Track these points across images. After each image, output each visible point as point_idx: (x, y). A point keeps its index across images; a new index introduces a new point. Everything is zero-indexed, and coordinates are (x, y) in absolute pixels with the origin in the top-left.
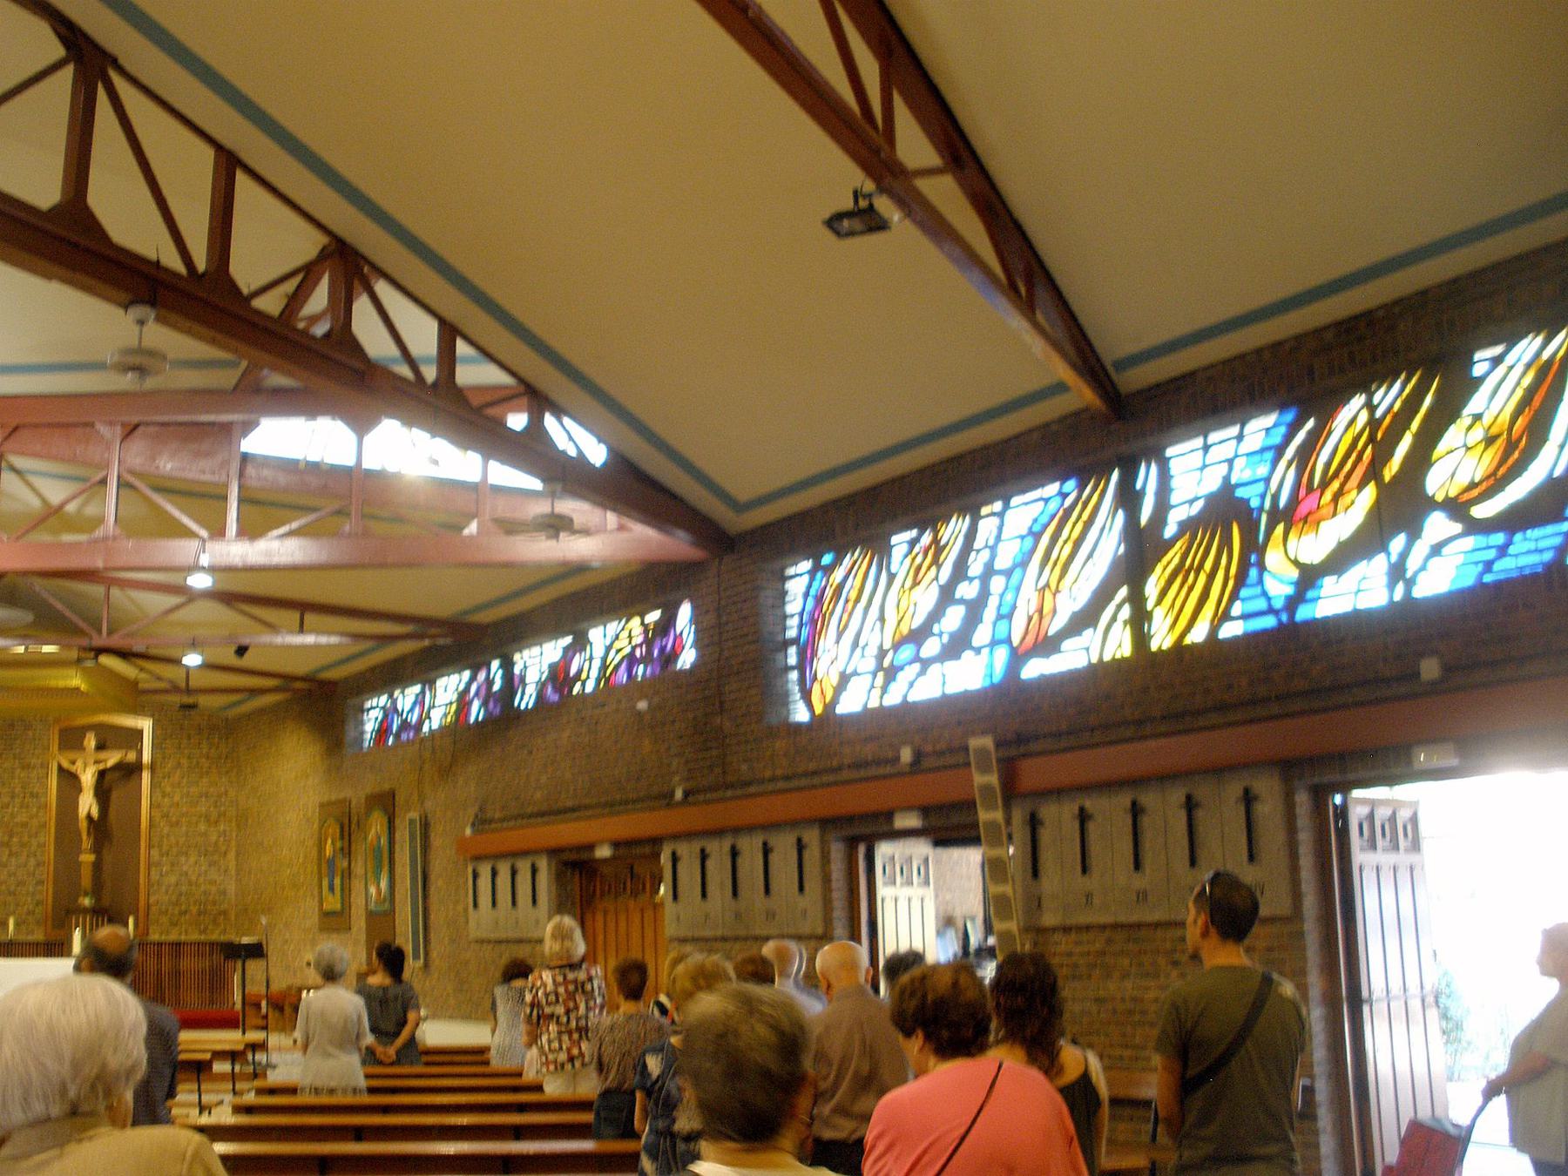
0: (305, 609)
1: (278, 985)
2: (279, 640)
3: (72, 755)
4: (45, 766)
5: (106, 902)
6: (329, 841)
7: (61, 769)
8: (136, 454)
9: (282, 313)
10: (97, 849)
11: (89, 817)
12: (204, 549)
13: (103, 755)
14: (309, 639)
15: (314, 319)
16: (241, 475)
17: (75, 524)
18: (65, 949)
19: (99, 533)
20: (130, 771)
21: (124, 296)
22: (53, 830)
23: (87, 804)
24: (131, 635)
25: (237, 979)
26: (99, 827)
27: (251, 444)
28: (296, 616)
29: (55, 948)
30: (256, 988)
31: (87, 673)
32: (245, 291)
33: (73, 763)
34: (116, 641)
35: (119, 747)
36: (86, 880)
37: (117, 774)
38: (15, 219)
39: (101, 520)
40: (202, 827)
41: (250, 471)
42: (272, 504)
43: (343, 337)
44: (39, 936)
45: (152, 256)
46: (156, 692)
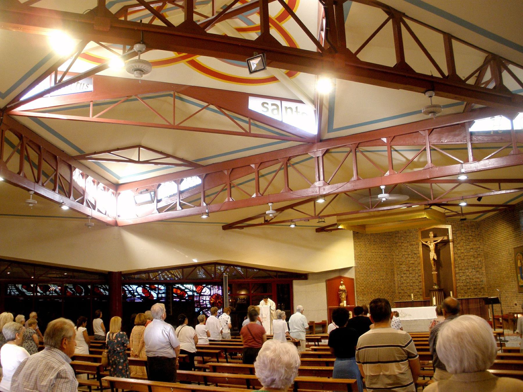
0: (500, 181)
1: (505, 312)
2: (492, 193)
3: (426, 240)
4: (418, 244)
5: (442, 287)
6: (519, 261)
7: (423, 244)
8: (434, 139)
9: (475, 83)
10: (437, 270)
11: (434, 259)
12: (463, 167)
13: (436, 239)
14: (504, 192)
15: (488, 83)
16: (471, 140)
17: (417, 165)
18: (430, 303)
19: (426, 167)
20: (446, 243)
21: (423, 90)
22: (422, 265)
23: (433, 255)
24: (441, 198)
25: (490, 311)
26: (437, 262)
27: (473, 129)
28: (497, 184)
29: (427, 303)
30: (498, 313)
31: (428, 213)
32: (463, 79)
33: (426, 242)
34: (436, 201)
35: (441, 236)
36: (435, 280)
37: (441, 245)
38: (383, 72)
39: (426, 162)
40: (472, 260)
41: (474, 138)
42: (483, 148)
43: (501, 87)
44: (421, 299)
45: (430, 74)
46: (450, 216)
